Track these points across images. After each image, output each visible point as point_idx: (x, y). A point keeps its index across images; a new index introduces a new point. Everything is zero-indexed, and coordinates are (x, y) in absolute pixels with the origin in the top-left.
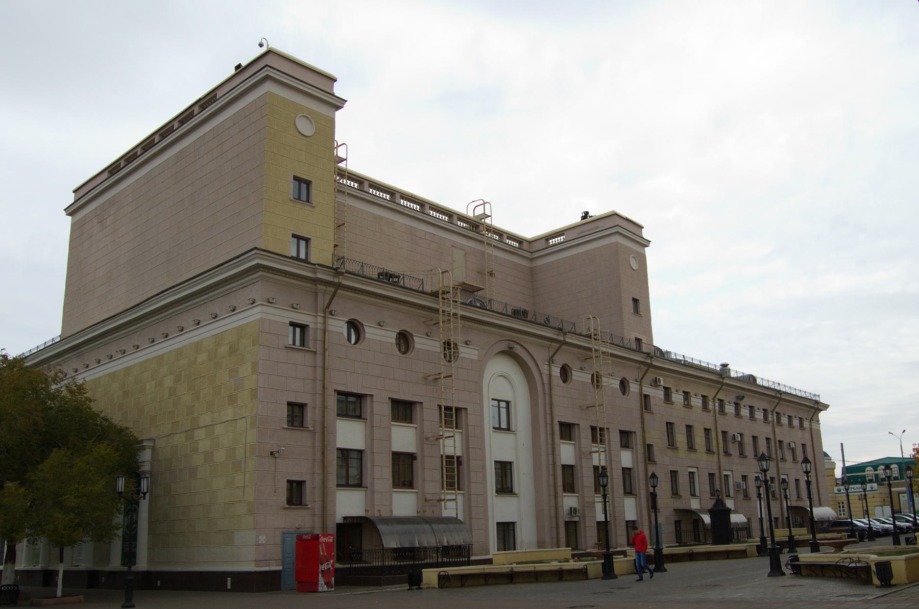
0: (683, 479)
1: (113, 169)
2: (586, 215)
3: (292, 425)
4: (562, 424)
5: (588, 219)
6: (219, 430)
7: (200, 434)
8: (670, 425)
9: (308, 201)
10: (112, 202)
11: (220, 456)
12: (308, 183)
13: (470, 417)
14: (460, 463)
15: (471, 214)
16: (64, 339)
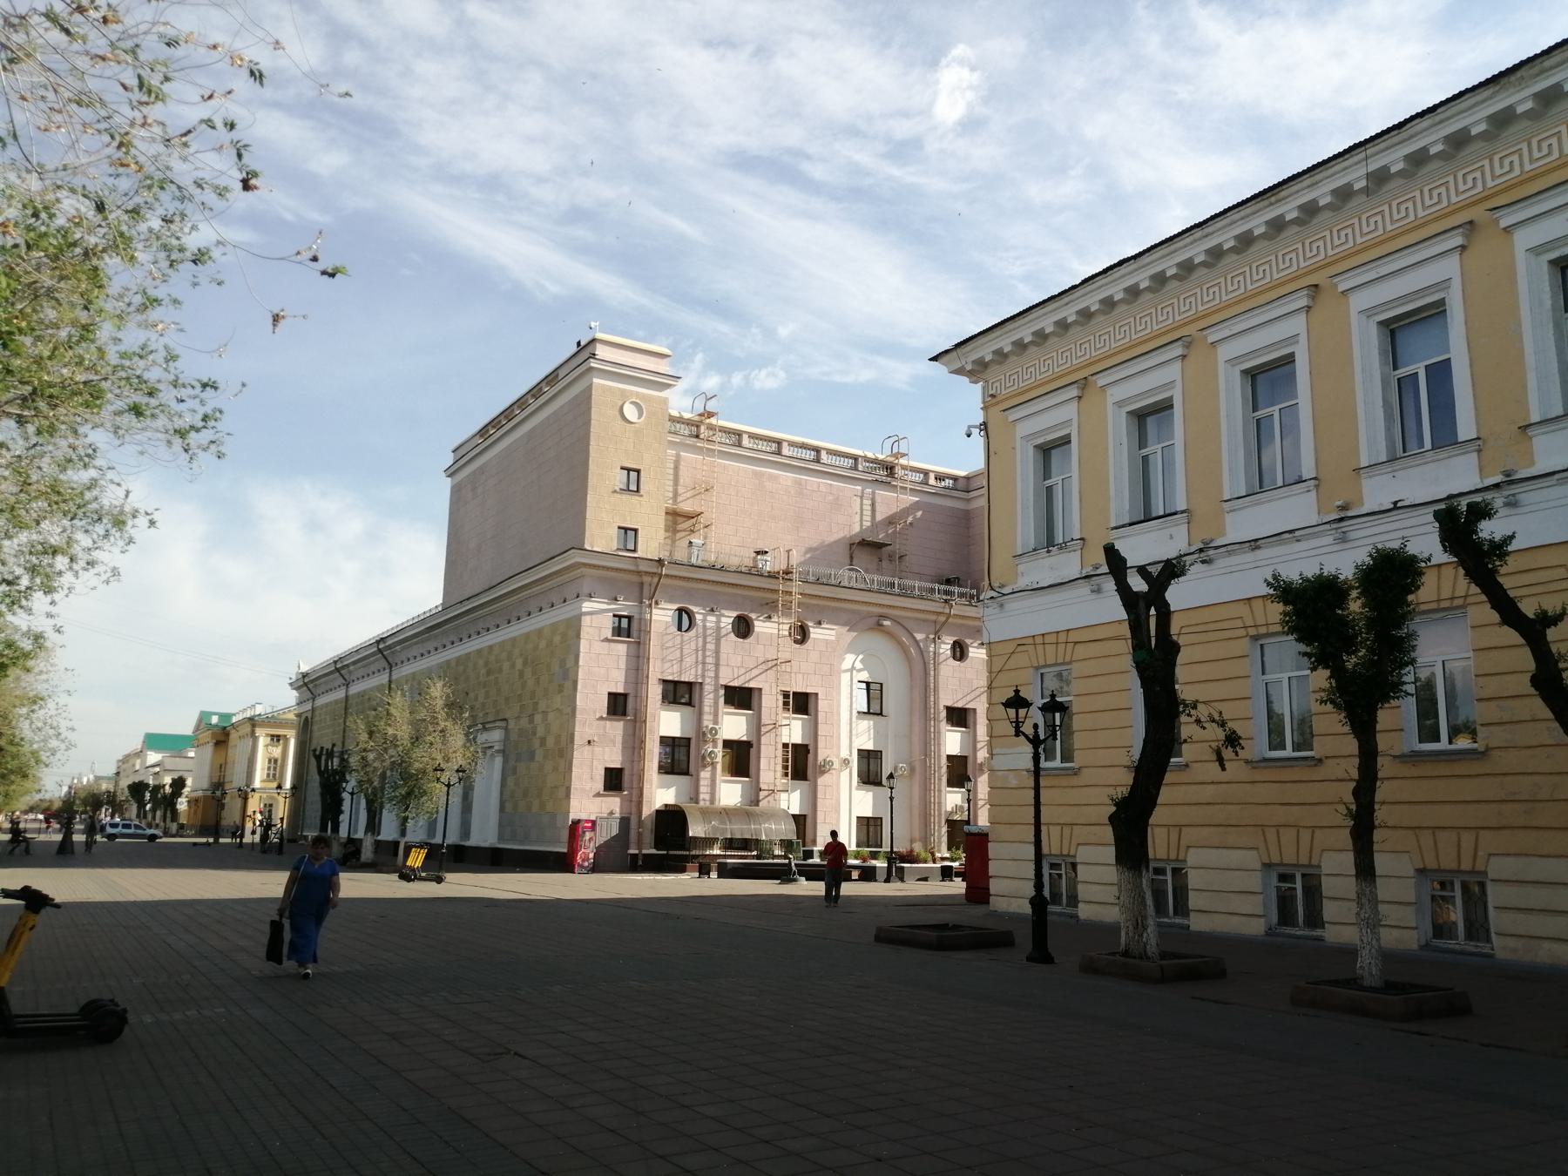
1: (483, 432)
4: (950, 710)
6: (551, 716)
7: (538, 718)
10: (481, 469)
11: (550, 742)
15: (881, 457)
16: (446, 607)
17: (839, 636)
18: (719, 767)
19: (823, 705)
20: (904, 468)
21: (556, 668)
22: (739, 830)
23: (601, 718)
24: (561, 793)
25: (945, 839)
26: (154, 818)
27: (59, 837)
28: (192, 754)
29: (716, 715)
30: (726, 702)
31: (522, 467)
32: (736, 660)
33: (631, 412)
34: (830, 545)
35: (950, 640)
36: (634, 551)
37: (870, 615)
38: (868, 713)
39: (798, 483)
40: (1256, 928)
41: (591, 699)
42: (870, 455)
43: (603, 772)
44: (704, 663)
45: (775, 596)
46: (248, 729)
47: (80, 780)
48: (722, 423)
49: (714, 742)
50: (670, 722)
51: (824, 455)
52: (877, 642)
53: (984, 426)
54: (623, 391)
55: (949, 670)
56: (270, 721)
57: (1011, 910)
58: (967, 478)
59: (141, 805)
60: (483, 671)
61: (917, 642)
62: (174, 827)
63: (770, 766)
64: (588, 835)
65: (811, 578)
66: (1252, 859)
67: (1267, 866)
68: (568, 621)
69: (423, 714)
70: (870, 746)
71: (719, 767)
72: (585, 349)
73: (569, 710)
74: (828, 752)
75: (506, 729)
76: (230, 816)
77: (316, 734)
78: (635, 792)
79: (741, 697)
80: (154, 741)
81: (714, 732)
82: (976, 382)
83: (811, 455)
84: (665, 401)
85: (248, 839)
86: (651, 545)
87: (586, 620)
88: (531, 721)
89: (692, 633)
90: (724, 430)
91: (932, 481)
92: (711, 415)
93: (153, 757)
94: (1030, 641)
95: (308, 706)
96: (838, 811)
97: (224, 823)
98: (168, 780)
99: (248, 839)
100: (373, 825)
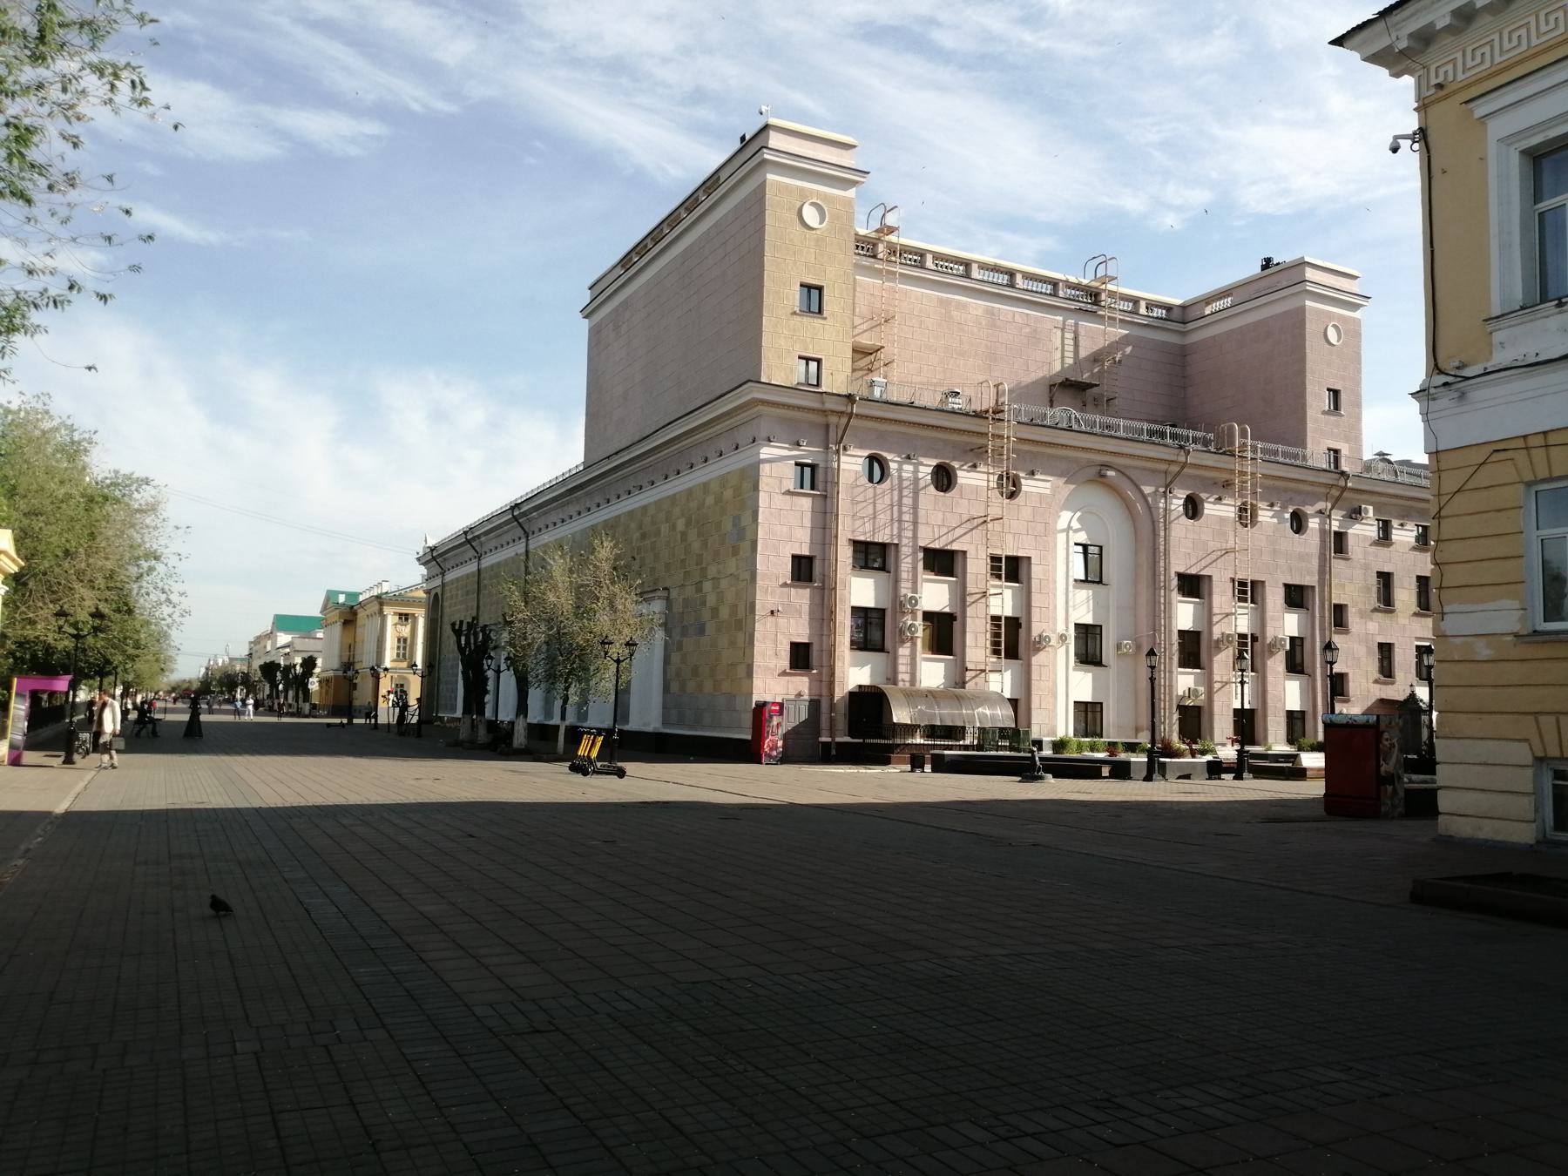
1: (625, 262)
2: (1267, 263)
3: (799, 580)
4: (1181, 576)
6: (724, 584)
7: (707, 586)
9: (820, 311)
10: (625, 304)
11: (724, 613)
12: (820, 289)
13: (1034, 568)
15: (1085, 282)
16: (588, 466)
17: (1054, 489)
18: (919, 643)
19: (1036, 571)
20: (1112, 294)
21: (728, 525)
22: (945, 715)
23: (785, 585)
24: (741, 671)
25: (1176, 727)
26: (286, 698)
27: (186, 717)
28: (320, 635)
29: (915, 582)
30: (926, 567)
31: (683, 292)
32: (937, 518)
33: (810, 215)
34: (1027, 386)
36: (818, 385)
37: (1090, 464)
38: (1086, 581)
39: (990, 312)
40: (1524, 834)
41: (772, 563)
42: (1072, 279)
43: (788, 648)
44: (900, 521)
45: (981, 441)
46: (376, 607)
47: (216, 662)
48: (904, 241)
49: (913, 613)
50: (862, 591)
51: (1019, 279)
52: (1099, 499)
53: (1422, 135)
54: (802, 189)
55: (1181, 527)
56: (398, 599)
57: (1482, 835)
58: (1183, 307)
59: (274, 686)
60: (637, 535)
61: (1144, 497)
62: (306, 708)
63: (976, 643)
64: (775, 720)
65: (1024, 419)
66: (1523, 754)
67: (1540, 761)
69: (588, 579)
70: (1089, 620)
71: (919, 643)
72: (752, 145)
73: (747, 576)
74: (1044, 626)
75: (668, 599)
76: (362, 697)
77: (447, 610)
78: (825, 670)
79: (942, 562)
80: (283, 622)
81: (914, 601)
82: (1397, 75)
83: (1004, 279)
85: (382, 719)
86: (837, 379)
87: (765, 469)
88: (699, 589)
89: (886, 485)
90: (906, 250)
91: (1143, 311)
92: (891, 230)
93: (283, 638)
94: (1521, 443)
95: (438, 582)
96: (1055, 695)
97: (356, 703)
98: (298, 660)
99: (382, 719)
100: (522, 708)
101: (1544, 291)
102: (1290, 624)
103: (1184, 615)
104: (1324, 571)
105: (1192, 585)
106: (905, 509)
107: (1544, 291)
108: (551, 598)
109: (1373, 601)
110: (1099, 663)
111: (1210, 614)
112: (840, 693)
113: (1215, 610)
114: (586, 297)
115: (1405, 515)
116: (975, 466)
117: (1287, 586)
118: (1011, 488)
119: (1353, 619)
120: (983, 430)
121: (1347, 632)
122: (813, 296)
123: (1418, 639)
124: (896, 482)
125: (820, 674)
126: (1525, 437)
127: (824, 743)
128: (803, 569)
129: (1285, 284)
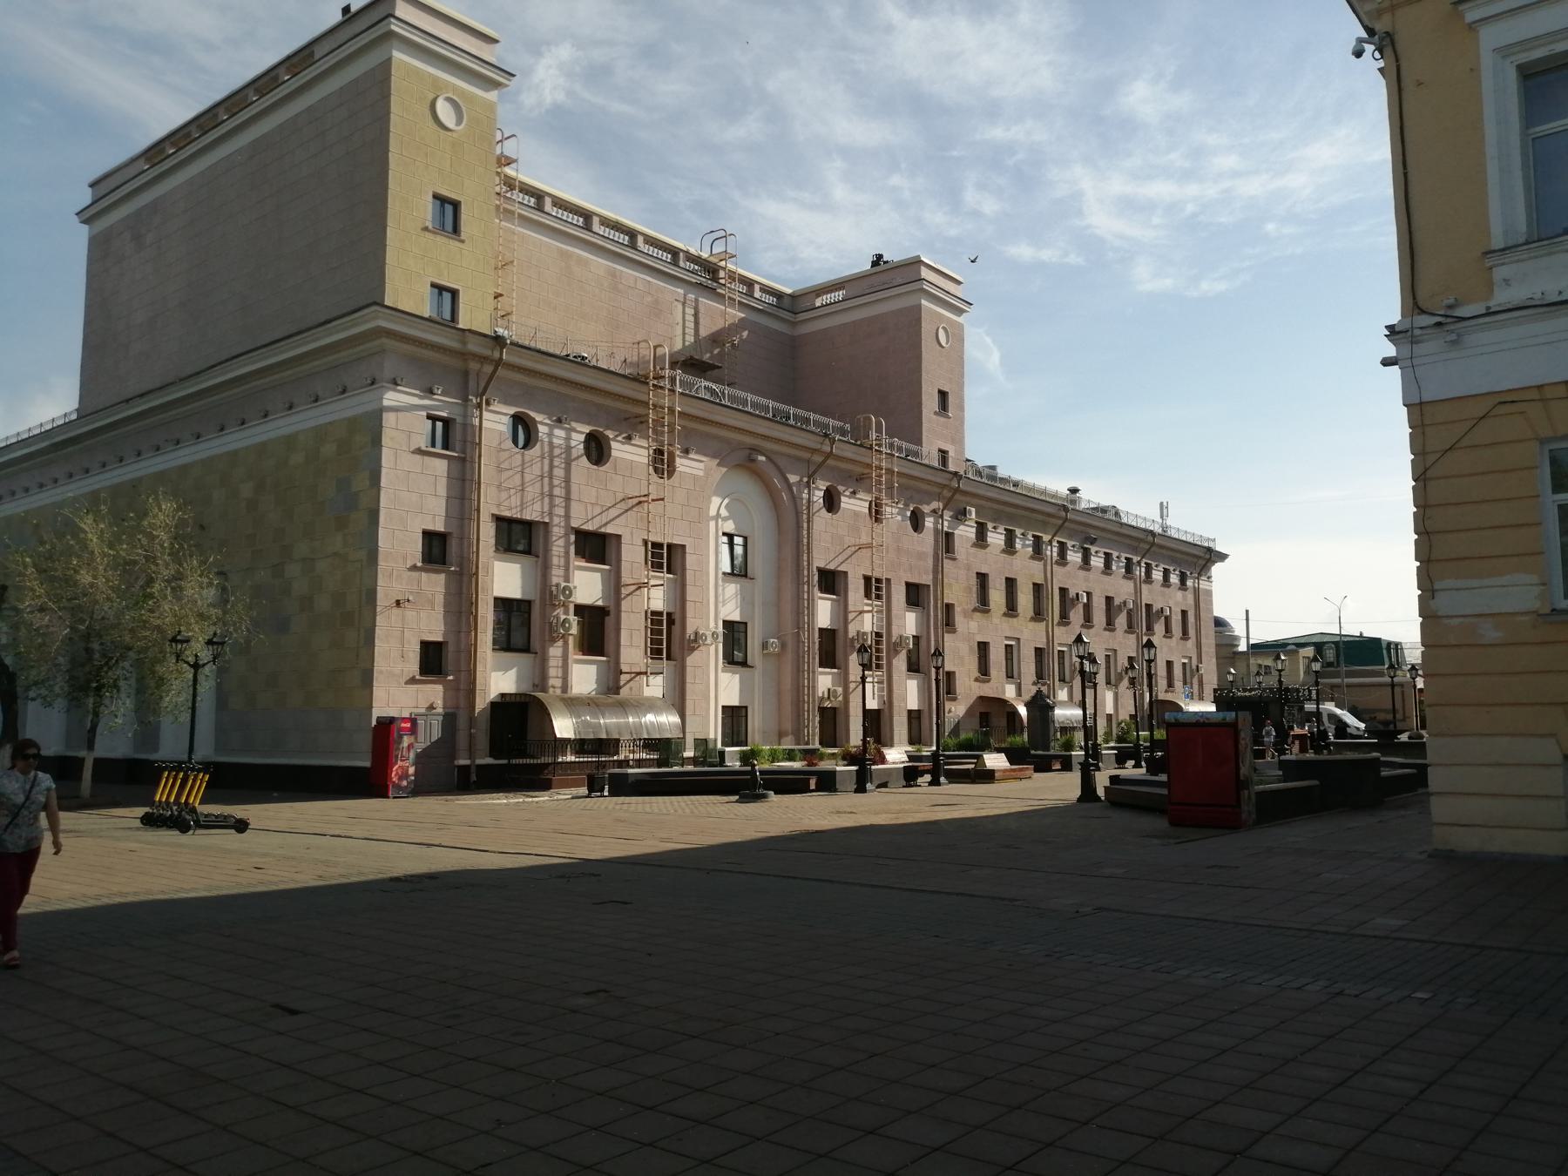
0: (997, 656)
4: (822, 572)
5: (882, 267)
7: (293, 570)
8: (982, 578)
9: (456, 230)
10: (154, 207)
11: (323, 603)
13: (689, 558)
14: (671, 621)
15: (705, 255)
16: (83, 413)
17: (707, 471)
18: (571, 640)
19: (690, 560)
20: (732, 276)
23: (414, 568)
29: (567, 569)
33: (444, 111)
35: (822, 485)
38: (732, 574)
42: (692, 251)
44: (551, 496)
45: (640, 410)
50: (506, 578)
52: (746, 486)
54: (436, 79)
55: (822, 518)
61: (789, 486)
63: (632, 646)
64: (406, 741)
68: (353, 424)
70: (736, 617)
71: (571, 640)
81: (568, 592)
84: (491, 107)
87: (389, 419)
89: (535, 451)
94: (1535, 395)
101: (1548, 230)
102: (909, 623)
103: (824, 612)
104: (938, 570)
105: (831, 581)
106: (556, 482)
107: (1548, 230)
108: (85, 578)
109: (974, 603)
110: (744, 664)
111: (846, 612)
112: (481, 704)
113: (851, 608)
114: (86, 197)
115: (997, 519)
116: (629, 438)
117: (908, 584)
118: (662, 464)
119: (959, 619)
120: (643, 397)
121: (954, 631)
122: (449, 213)
123: (1007, 638)
124: (546, 449)
125: (457, 680)
126: (1540, 387)
127: (460, 767)
128: (436, 549)
129: (900, 281)
